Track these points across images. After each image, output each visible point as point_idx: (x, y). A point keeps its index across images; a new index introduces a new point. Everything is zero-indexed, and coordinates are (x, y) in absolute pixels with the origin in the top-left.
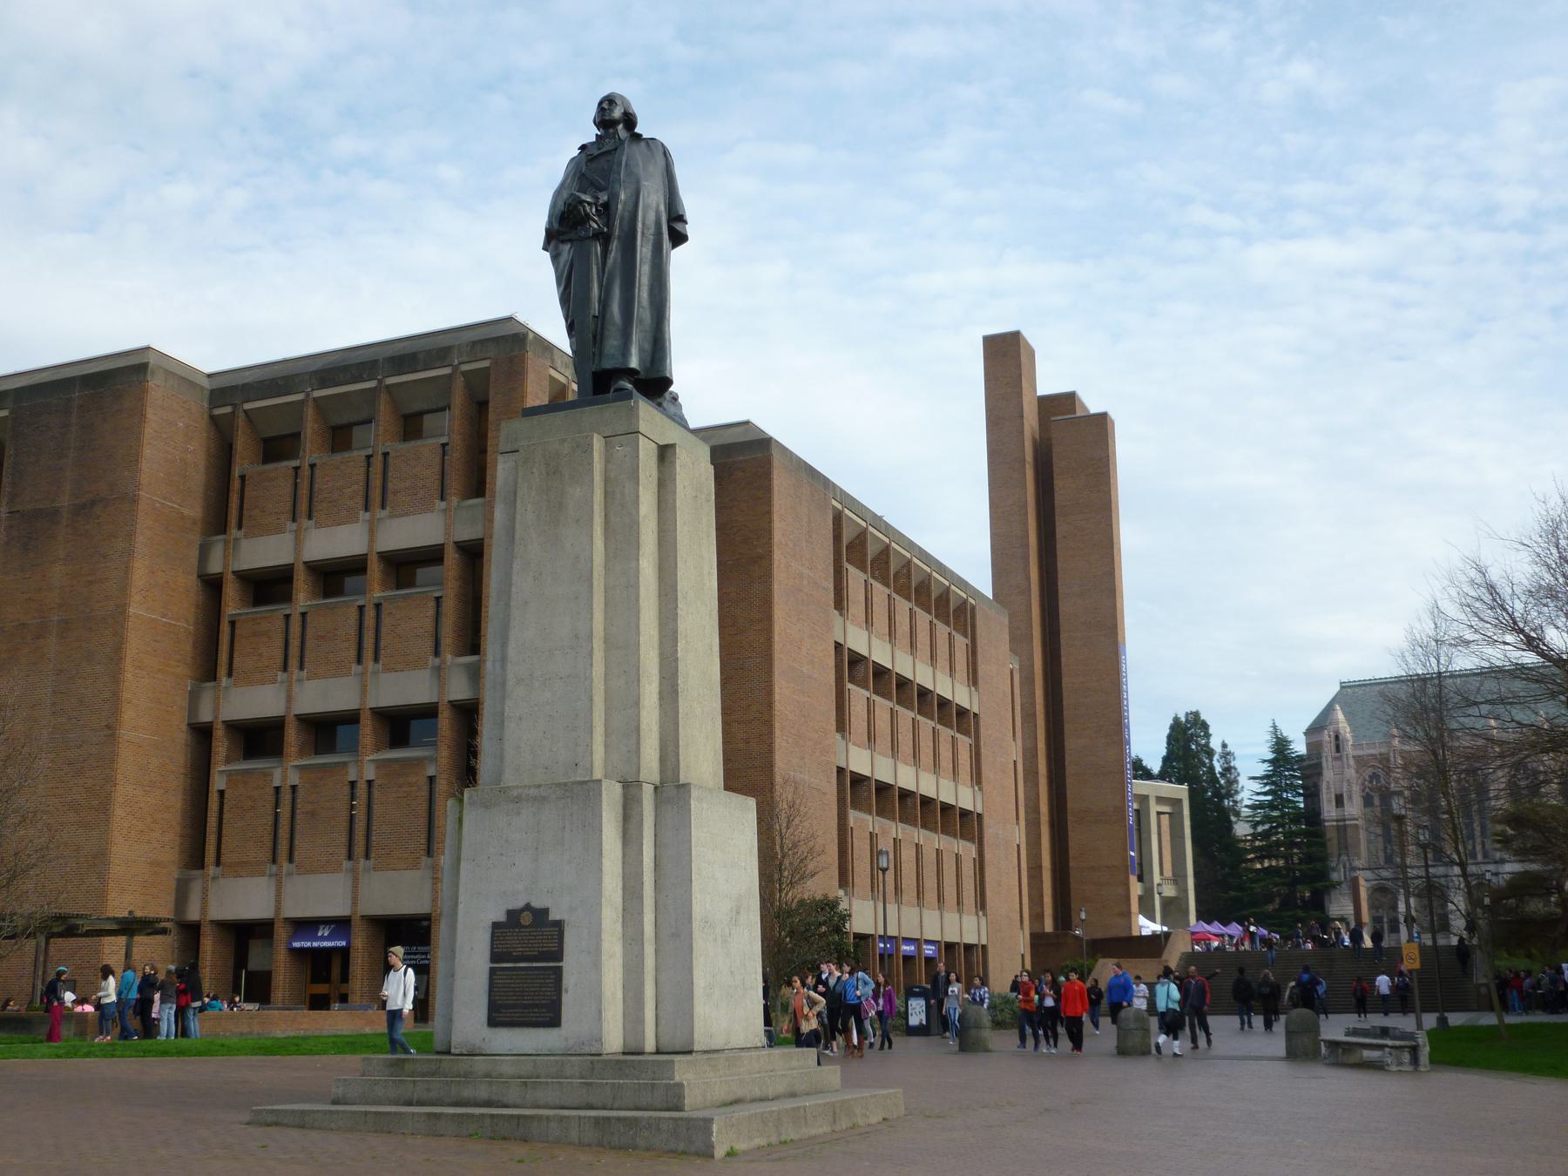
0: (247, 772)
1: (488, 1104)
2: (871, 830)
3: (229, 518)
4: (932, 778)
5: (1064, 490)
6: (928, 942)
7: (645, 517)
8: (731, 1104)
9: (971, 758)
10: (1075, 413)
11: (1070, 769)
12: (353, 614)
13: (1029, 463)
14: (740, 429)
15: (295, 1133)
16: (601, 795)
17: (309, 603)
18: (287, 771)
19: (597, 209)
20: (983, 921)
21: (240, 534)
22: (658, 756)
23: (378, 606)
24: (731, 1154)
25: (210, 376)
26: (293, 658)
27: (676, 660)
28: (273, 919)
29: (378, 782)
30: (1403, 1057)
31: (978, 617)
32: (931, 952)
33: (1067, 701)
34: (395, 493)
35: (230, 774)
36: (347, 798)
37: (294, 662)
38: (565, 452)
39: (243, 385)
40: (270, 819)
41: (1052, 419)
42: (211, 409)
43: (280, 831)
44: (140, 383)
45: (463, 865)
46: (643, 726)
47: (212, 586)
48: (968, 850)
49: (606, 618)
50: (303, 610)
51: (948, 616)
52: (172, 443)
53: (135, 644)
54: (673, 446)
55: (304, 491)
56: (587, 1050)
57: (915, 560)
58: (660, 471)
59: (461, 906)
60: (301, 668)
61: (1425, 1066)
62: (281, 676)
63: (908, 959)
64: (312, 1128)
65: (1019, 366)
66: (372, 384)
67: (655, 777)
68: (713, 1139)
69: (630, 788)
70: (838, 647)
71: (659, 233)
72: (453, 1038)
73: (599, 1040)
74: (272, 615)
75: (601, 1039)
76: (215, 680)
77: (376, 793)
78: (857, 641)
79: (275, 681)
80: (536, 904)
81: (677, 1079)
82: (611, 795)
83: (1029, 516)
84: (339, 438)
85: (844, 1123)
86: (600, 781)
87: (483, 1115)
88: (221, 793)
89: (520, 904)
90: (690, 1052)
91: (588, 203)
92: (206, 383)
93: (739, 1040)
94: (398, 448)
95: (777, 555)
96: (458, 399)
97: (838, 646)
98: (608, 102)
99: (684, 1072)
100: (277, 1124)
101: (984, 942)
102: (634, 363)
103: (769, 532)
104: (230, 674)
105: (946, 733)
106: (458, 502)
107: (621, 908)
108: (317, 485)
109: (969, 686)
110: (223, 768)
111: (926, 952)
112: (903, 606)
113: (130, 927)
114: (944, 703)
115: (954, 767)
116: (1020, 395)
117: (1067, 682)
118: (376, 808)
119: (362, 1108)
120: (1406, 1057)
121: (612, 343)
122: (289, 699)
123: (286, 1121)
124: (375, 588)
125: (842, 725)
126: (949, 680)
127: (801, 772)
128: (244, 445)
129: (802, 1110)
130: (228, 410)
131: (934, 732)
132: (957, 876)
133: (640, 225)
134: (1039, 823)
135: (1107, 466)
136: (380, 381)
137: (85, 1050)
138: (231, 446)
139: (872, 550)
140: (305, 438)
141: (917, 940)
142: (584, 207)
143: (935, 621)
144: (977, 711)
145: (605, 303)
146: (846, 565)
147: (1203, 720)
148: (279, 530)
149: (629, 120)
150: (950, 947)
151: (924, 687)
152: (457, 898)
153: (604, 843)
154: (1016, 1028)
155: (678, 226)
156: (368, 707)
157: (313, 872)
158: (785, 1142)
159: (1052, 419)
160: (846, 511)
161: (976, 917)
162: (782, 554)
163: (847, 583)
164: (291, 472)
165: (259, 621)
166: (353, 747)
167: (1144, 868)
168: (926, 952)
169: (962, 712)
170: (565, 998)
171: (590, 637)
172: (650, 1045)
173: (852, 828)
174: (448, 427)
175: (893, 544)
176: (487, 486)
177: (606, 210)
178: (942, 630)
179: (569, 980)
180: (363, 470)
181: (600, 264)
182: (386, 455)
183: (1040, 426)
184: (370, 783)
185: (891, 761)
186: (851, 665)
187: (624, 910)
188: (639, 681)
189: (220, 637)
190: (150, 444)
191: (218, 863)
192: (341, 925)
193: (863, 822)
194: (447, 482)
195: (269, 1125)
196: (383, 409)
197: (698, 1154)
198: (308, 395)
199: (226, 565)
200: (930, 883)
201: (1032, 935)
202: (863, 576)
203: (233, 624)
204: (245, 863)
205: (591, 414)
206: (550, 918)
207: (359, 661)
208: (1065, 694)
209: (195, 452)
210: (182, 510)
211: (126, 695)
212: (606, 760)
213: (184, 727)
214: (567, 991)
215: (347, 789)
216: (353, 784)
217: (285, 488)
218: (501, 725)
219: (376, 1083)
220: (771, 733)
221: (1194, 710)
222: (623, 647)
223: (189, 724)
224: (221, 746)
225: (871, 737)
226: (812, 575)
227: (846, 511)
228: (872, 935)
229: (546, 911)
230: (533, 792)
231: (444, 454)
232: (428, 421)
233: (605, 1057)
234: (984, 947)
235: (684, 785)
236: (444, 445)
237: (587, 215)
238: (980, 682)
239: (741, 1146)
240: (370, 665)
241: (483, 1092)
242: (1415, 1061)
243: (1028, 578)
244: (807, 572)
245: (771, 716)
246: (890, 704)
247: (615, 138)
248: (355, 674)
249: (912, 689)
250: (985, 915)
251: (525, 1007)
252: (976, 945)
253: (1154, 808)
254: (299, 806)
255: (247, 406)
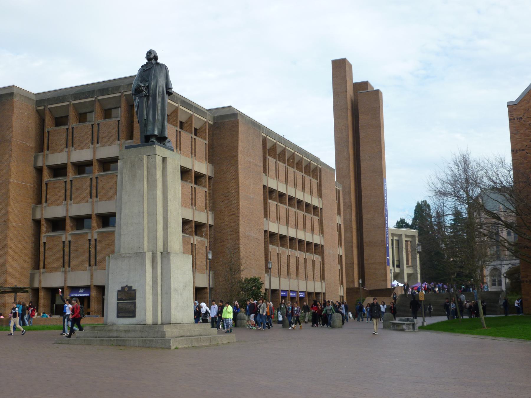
0: (53, 236)
1: (117, 337)
2: (278, 252)
3: (44, 147)
4: (303, 233)
5: (363, 119)
6: (301, 292)
7: (158, 178)
8: (180, 337)
9: (319, 224)
10: (367, 89)
11: (365, 227)
12: (88, 180)
13: (349, 109)
14: (228, 109)
15: (67, 346)
16: (145, 256)
17: (73, 177)
18: (67, 236)
19: (145, 88)
20: (324, 284)
21: (48, 152)
22: (162, 245)
23: (97, 178)
24: (176, 348)
25: (35, 94)
26: (68, 196)
27: (167, 218)
28: (64, 287)
29: (98, 240)
30: (410, 327)
31: (322, 172)
32: (302, 296)
33: (364, 200)
34: (102, 138)
35: (47, 237)
36: (88, 245)
37: (68, 198)
38: (136, 160)
39: (48, 99)
40: (62, 253)
41: (358, 92)
42: (36, 108)
43: (65, 256)
44: (11, 100)
45: (110, 275)
46: (158, 237)
47: (39, 170)
48: (317, 258)
49: (148, 207)
50: (71, 179)
51: (310, 173)
52: (23, 120)
53: (13, 192)
54: (166, 158)
55: (70, 137)
56: (142, 323)
57: (296, 153)
58: (163, 165)
59: (109, 286)
60: (71, 200)
61: (417, 330)
62: (64, 202)
63: (293, 298)
64: (71, 344)
65: (345, 72)
66: (93, 99)
67: (162, 250)
68: (171, 344)
69: (154, 253)
70: (265, 187)
71: (163, 94)
72: (108, 321)
73: (145, 321)
74: (61, 180)
75: (146, 321)
76: (41, 204)
77: (98, 243)
78: (272, 184)
79: (62, 205)
80: (129, 285)
81: (164, 330)
82: (148, 256)
83: (349, 130)
84: (82, 118)
85: (214, 343)
86: (145, 252)
87: (114, 340)
88: (45, 243)
89: (125, 285)
90: (170, 324)
91: (143, 86)
92: (34, 98)
93: (185, 321)
94: (101, 121)
95: (240, 155)
96: (123, 104)
97: (265, 187)
98: (150, 53)
99: (167, 329)
100: (61, 343)
101: (324, 291)
102: (156, 133)
103: (237, 147)
104: (46, 202)
105: (308, 216)
106: (124, 141)
107: (152, 286)
108: (74, 135)
109: (318, 198)
110: (45, 235)
111: (300, 295)
112: (291, 170)
113: (15, 290)
114: (308, 205)
115: (312, 228)
116: (346, 83)
117: (363, 193)
118: (98, 248)
119: (84, 339)
120: (411, 327)
121: (150, 127)
122: (67, 211)
123: (64, 342)
124: (96, 171)
125: (266, 215)
126: (310, 196)
127: (250, 233)
128: (49, 121)
129: (200, 339)
130: (42, 108)
131: (304, 216)
132: (313, 268)
133: (157, 92)
134: (353, 247)
135: (379, 110)
136: (96, 98)
137: (5, 329)
138: (44, 120)
139: (278, 151)
140: (70, 118)
141: (297, 291)
142: (141, 88)
143: (304, 175)
144: (321, 207)
145: (148, 115)
146: (268, 157)
147: (428, 204)
148: (62, 151)
149: (156, 58)
150: (310, 294)
151: (299, 199)
152: (108, 284)
153: (146, 269)
154: (310, 322)
155: (169, 91)
156: (94, 213)
157: (77, 270)
158: (194, 346)
159: (358, 92)
160: (268, 137)
161: (320, 283)
162: (242, 155)
163: (268, 163)
164: (66, 130)
165: (56, 183)
166: (90, 227)
167: (400, 262)
168: (300, 295)
169: (315, 208)
170: (137, 310)
171: (143, 213)
172: (160, 322)
173: (270, 252)
174: (120, 114)
175: (287, 148)
176: (134, 136)
177: (148, 87)
178: (307, 178)
179: (138, 305)
180: (91, 130)
181: (146, 104)
182: (98, 124)
183: (354, 96)
184: (96, 240)
185: (286, 227)
186: (270, 193)
187: (153, 287)
188: (156, 224)
189: (42, 189)
190: (15, 121)
191: (44, 268)
192: (87, 288)
193: (274, 249)
194: (120, 134)
195: (59, 344)
196: (97, 109)
197: (167, 348)
198: (70, 103)
199: (44, 163)
200: (302, 270)
201: (347, 289)
202: (274, 160)
203: (47, 184)
204: (54, 267)
205: (143, 149)
206: (133, 289)
207: (91, 197)
208: (363, 198)
209: (32, 123)
210: (27, 144)
211: (11, 210)
212: (148, 246)
213: (31, 221)
214: (137, 308)
215: (88, 242)
216: (90, 240)
217: (64, 136)
218: (120, 236)
219: (88, 332)
220: (238, 219)
221: (425, 200)
222: (152, 215)
223: (32, 220)
224: (44, 227)
225: (278, 219)
226: (254, 162)
227: (268, 137)
228: (278, 290)
229: (131, 287)
230: (128, 255)
231: (119, 124)
232: (113, 112)
233: (147, 325)
234: (324, 293)
235: (169, 253)
236: (118, 121)
237: (142, 90)
238: (323, 196)
239: (180, 347)
240: (95, 199)
241: (115, 334)
242: (414, 328)
243: (349, 154)
244: (252, 160)
245: (238, 213)
246: (285, 206)
247: (151, 64)
248: (90, 202)
249: (295, 200)
250: (324, 282)
251: (126, 312)
252: (321, 293)
253: (404, 239)
254: (71, 248)
255: (49, 106)
